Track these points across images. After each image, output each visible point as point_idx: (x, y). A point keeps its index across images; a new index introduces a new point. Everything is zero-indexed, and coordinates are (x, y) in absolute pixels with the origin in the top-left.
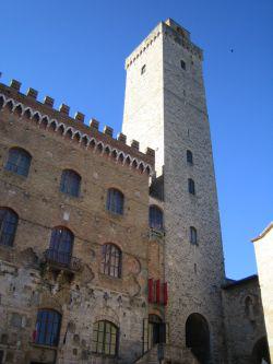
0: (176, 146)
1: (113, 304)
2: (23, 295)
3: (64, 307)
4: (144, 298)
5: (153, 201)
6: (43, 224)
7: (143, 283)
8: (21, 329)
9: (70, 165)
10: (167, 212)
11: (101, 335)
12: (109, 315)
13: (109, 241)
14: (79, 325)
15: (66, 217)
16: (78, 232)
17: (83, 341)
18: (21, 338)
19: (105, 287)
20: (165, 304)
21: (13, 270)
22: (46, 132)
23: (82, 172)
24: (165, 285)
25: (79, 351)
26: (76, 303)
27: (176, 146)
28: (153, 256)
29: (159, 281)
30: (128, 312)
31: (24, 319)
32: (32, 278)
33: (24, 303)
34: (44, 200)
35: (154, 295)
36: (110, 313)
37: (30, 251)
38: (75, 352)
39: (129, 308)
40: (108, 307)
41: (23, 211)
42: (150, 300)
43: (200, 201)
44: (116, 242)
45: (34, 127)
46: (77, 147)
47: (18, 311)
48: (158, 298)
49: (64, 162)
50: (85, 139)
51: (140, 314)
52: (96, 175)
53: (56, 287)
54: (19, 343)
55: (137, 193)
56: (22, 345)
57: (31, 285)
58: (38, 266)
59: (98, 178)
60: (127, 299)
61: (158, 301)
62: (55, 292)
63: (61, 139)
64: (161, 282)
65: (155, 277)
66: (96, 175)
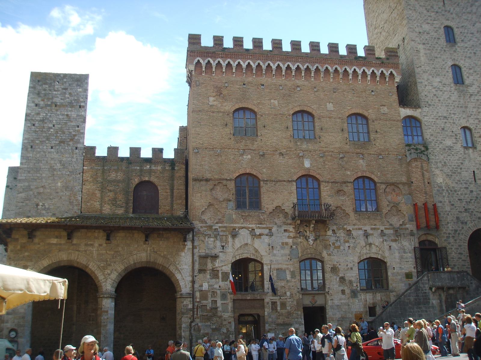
0: (426, 27)
1: (376, 240)
2: (282, 252)
3: (325, 254)
4: (411, 226)
5: (405, 112)
6: (285, 178)
7: (407, 209)
8: (288, 281)
9: (319, 174)
10: (425, 120)
11: (355, 135)
12: (374, 253)
13: (360, 175)
14: (342, 267)
15: (307, 164)
16: (323, 175)
17: (351, 282)
18: (289, 289)
19: (365, 225)
20: (437, 227)
21: (267, 231)
22: (264, 79)
23: (313, 108)
24: (435, 205)
25: (347, 291)
26: (335, 248)
27: (426, 27)
28: (416, 177)
29: (425, 204)
30: (394, 245)
31: (288, 272)
32: (287, 234)
33: (284, 258)
34: (281, 154)
35: (423, 221)
36: (374, 249)
37: (278, 209)
38: (343, 292)
39: (395, 241)
40: (370, 244)
41: (263, 173)
42: (418, 227)
43: (471, 90)
44: (368, 174)
45: (250, 79)
46: (301, 82)
47: (280, 266)
48: (427, 222)
49: (291, 106)
50: (308, 69)
51: (409, 244)
52: (330, 106)
53: (312, 238)
54: (288, 294)
55: (385, 110)
56: (292, 294)
57: (287, 240)
58: (289, 221)
59: (331, 104)
60: (391, 231)
61: (428, 226)
62: (311, 242)
63: (282, 80)
64: (430, 206)
65: (420, 200)
66: (330, 106)
